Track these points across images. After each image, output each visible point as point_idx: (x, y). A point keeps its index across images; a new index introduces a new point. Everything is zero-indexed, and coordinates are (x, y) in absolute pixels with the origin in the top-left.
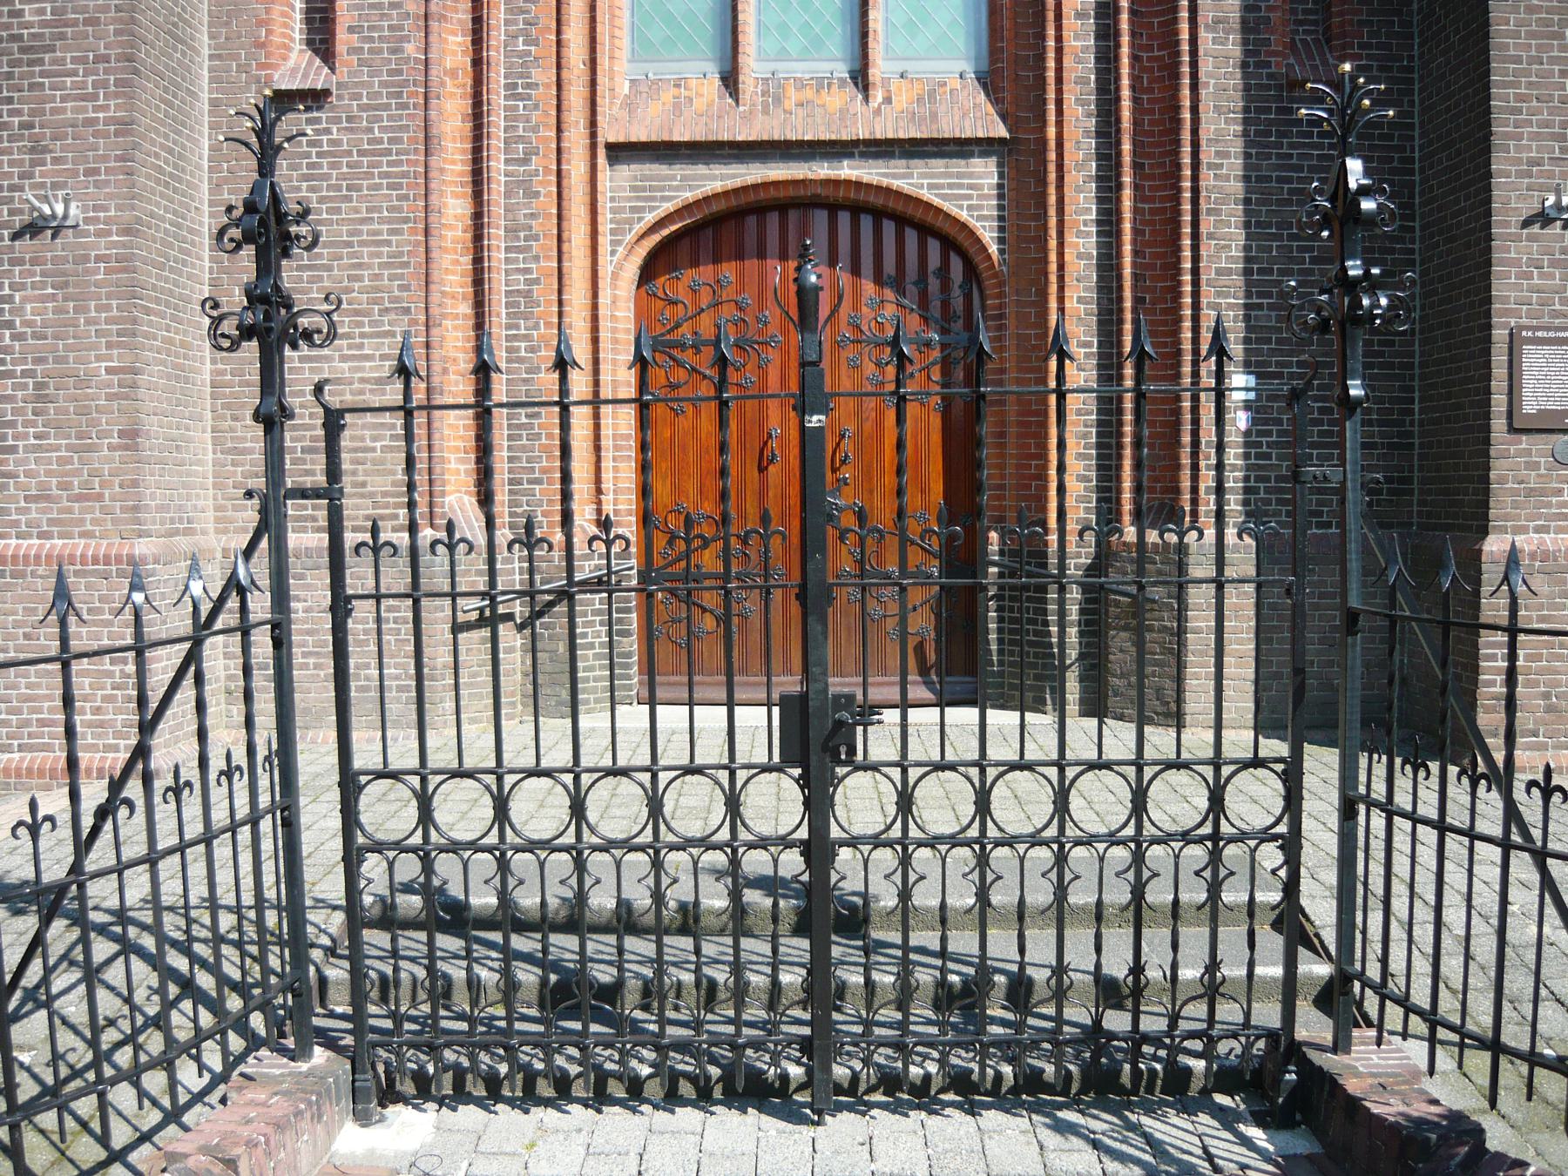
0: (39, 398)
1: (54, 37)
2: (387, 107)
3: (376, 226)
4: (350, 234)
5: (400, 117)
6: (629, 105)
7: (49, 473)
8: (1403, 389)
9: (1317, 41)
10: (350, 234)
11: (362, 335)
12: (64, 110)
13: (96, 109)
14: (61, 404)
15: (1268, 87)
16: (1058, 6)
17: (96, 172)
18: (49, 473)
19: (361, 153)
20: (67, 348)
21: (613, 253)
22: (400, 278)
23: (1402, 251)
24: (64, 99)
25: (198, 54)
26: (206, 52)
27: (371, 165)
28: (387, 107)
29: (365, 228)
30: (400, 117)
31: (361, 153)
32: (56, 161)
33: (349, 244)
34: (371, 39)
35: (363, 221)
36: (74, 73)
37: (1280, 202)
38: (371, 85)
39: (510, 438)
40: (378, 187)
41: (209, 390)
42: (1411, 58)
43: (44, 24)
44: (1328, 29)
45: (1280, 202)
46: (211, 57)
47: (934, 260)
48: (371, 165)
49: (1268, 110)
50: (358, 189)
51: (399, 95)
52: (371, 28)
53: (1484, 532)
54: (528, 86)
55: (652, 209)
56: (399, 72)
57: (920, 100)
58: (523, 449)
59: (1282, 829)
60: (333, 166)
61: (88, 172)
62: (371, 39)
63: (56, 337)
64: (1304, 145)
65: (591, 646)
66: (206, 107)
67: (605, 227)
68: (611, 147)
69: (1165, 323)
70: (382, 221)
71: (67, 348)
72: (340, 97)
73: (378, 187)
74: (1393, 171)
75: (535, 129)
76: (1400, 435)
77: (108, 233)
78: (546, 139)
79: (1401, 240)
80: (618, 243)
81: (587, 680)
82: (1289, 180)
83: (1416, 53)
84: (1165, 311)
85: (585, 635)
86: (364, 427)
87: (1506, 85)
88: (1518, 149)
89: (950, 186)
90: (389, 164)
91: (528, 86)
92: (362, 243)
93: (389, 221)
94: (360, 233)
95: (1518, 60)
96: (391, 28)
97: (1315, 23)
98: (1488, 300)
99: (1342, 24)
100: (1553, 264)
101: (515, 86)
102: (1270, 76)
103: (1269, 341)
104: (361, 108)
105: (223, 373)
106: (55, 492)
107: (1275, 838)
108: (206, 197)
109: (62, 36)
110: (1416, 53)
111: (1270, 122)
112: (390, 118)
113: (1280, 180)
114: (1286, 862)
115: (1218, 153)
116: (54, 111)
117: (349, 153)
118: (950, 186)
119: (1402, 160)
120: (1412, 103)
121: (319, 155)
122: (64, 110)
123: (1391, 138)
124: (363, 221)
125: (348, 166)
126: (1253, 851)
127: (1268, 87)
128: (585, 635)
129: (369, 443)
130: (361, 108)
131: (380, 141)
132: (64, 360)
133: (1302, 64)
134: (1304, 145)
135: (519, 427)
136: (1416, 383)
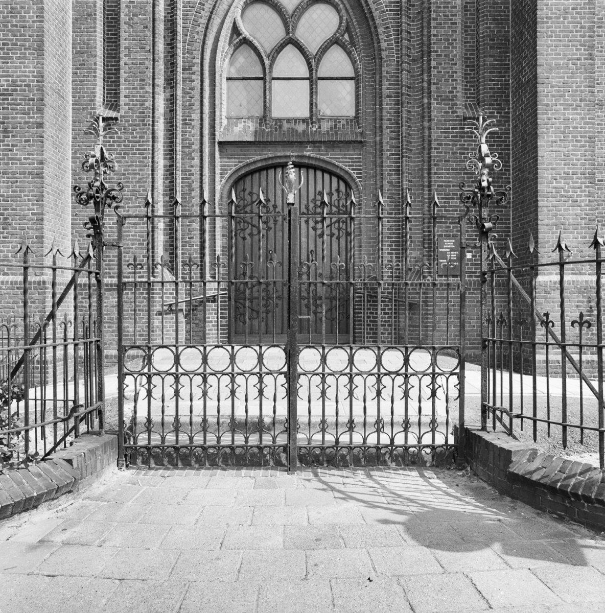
0: (5, 224)
1: (13, 90)
2: (139, 125)
3: (134, 168)
4: (125, 170)
5: (144, 129)
6: (227, 128)
7: (8, 251)
8: (506, 227)
9: (474, 104)
10: (125, 170)
11: (129, 207)
12: (17, 118)
13: (29, 118)
14: (14, 225)
15: (456, 120)
16: (366, 2)
17: (29, 141)
18: (8, 251)
19: (129, 141)
20: (17, 206)
21: (221, 181)
22: (144, 186)
23: (505, 178)
24: (16, 114)
25: (68, 103)
26: (71, 102)
27: (133, 146)
28: (139, 125)
29: (130, 168)
30: (144, 129)
31: (129, 141)
32: (13, 136)
33: (124, 174)
34: (133, 101)
35: (129, 166)
36: (21, 104)
37: (460, 161)
38: (133, 117)
39: (182, 246)
40: (135, 154)
41: (70, 226)
42: (509, 109)
43: (8, 85)
44: (478, 100)
45: (460, 161)
46: (73, 104)
47: (335, 185)
48: (133, 146)
49: (456, 128)
50: (128, 154)
51: (143, 121)
52: (133, 96)
53: (537, 275)
54: (190, 120)
55: (235, 165)
56: (144, 113)
57: (331, 128)
58: (187, 250)
59: (458, 371)
60: (119, 146)
61: (26, 141)
62: (133, 101)
63: (12, 201)
64: (469, 141)
65: (211, 322)
66: (71, 123)
67: (218, 171)
68: (220, 143)
69: (419, 206)
70: (136, 166)
71: (17, 206)
72: (121, 121)
73: (135, 154)
74: (502, 149)
75: (193, 136)
76: (506, 227)
77: (33, 164)
78: (197, 139)
79: (505, 174)
80: (223, 177)
81: (209, 334)
82: (464, 154)
83: (511, 106)
84: (419, 202)
85: (209, 318)
86: (129, 240)
87: (543, 114)
88: (548, 137)
89: (342, 158)
90: (139, 146)
91: (190, 120)
92: (129, 174)
93: (140, 166)
94: (128, 170)
95: (548, 105)
96: (140, 96)
97: (474, 98)
98: (537, 192)
99: (483, 97)
100: (561, 178)
101: (186, 120)
102: (457, 116)
103: (456, 211)
104: (130, 125)
105: (76, 220)
106: (10, 258)
107: (455, 374)
108: (71, 155)
109: (16, 90)
110: (511, 106)
111: (457, 133)
112: (140, 129)
113: (460, 153)
114: (459, 383)
115: (438, 144)
116: (12, 118)
117: (125, 141)
118: (342, 158)
119: (505, 146)
120: (509, 125)
121: (113, 142)
122: (17, 118)
123: (501, 138)
124: (129, 166)
125: (124, 146)
126: (447, 379)
127: (456, 120)
128: (209, 318)
129: (130, 246)
130: (130, 125)
131: (136, 137)
132: (15, 210)
133: (469, 112)
134: (469, 141)
135: (186, 242)
136: (511, 225)
